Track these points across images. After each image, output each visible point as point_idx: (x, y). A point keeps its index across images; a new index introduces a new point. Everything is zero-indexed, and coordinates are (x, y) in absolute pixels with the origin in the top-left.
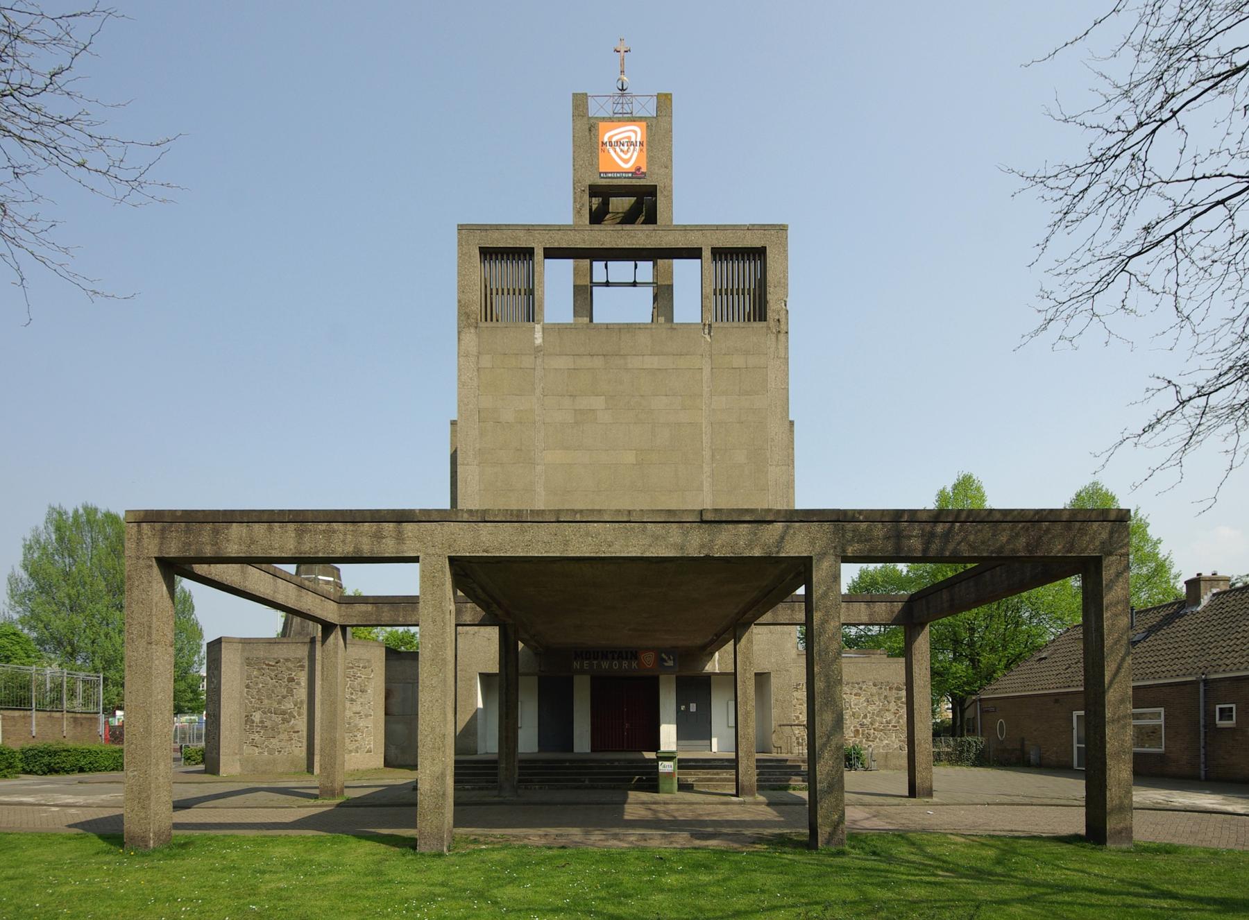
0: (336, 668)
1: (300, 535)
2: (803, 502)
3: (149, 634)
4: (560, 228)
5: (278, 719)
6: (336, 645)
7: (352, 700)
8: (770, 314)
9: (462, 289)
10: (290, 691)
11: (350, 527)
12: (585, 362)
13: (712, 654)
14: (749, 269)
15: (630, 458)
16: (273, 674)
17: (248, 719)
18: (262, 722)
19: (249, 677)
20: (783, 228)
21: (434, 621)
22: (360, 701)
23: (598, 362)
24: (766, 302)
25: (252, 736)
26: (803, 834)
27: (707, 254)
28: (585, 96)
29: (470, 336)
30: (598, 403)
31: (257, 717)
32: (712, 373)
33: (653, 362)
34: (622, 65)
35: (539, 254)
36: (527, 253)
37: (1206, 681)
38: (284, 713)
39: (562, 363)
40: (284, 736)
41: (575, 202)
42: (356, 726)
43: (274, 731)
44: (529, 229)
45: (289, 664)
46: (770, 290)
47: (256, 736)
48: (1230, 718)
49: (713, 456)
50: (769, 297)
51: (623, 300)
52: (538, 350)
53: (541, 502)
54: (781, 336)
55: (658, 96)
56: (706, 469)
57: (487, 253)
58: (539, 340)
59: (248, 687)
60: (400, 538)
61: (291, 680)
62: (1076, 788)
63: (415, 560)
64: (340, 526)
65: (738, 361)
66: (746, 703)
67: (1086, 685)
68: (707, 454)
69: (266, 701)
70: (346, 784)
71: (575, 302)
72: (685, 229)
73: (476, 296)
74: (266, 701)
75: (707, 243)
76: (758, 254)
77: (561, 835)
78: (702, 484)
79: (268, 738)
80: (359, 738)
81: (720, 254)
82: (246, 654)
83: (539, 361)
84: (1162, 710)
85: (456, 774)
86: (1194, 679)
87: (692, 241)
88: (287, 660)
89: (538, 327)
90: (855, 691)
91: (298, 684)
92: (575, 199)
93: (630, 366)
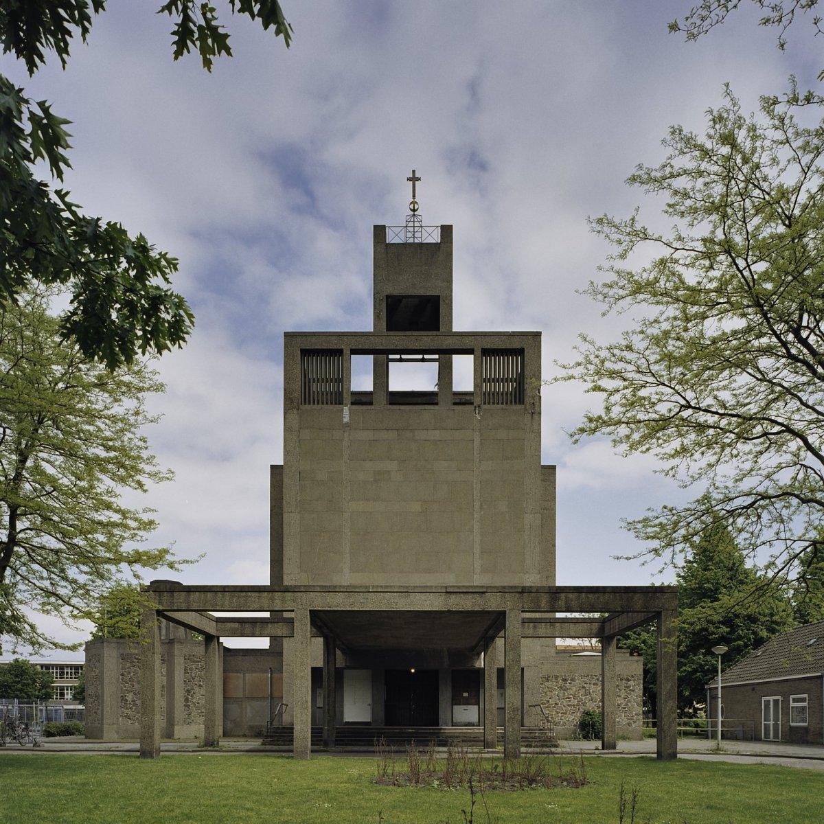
1: (535, 627)
3: (153, 648)
6: (214, 648)
7: (200, 686)
8: (526, 399)
11: (257, 594)
13: (479, 655)
14: (510, 367)
15: (416, 507)
18: (133, 701)
20: (537, 335)
21: (302, 643)
23: (392, 435)
24: (524, 390)
26: (498, 752)
27: (478, 353)
28: (384, 227)
29: (294, 415)
30: (393, 466)
31: (130, 697)
32: (481, 444)
33: (436, 435)
35: (347, 352)
36: (339, 352)
39: (366, 435)
41: (375, 309)
46: (527, 381)
47: (130, 712)
48: (793, 699)
50: (526, 386)
51: (411, 376)
52: (347, 425)
54: (535, 416)
55: (443, 227)
56: (476, 515)
57: (306, 353)
59: (122, 675)
60: (284, 600)
63: (293, 611)
64: (253, 594)
65: (502, 434)
66: (491, 689)
73: (297, 385)
75: (478, 345)
76: (520, 352)
78: (472, 526)
81: (487, 352)
83: (346, 434)
84: (806, 696)
86: (820, 674)
87: (468, 343)
90: (593, 682)
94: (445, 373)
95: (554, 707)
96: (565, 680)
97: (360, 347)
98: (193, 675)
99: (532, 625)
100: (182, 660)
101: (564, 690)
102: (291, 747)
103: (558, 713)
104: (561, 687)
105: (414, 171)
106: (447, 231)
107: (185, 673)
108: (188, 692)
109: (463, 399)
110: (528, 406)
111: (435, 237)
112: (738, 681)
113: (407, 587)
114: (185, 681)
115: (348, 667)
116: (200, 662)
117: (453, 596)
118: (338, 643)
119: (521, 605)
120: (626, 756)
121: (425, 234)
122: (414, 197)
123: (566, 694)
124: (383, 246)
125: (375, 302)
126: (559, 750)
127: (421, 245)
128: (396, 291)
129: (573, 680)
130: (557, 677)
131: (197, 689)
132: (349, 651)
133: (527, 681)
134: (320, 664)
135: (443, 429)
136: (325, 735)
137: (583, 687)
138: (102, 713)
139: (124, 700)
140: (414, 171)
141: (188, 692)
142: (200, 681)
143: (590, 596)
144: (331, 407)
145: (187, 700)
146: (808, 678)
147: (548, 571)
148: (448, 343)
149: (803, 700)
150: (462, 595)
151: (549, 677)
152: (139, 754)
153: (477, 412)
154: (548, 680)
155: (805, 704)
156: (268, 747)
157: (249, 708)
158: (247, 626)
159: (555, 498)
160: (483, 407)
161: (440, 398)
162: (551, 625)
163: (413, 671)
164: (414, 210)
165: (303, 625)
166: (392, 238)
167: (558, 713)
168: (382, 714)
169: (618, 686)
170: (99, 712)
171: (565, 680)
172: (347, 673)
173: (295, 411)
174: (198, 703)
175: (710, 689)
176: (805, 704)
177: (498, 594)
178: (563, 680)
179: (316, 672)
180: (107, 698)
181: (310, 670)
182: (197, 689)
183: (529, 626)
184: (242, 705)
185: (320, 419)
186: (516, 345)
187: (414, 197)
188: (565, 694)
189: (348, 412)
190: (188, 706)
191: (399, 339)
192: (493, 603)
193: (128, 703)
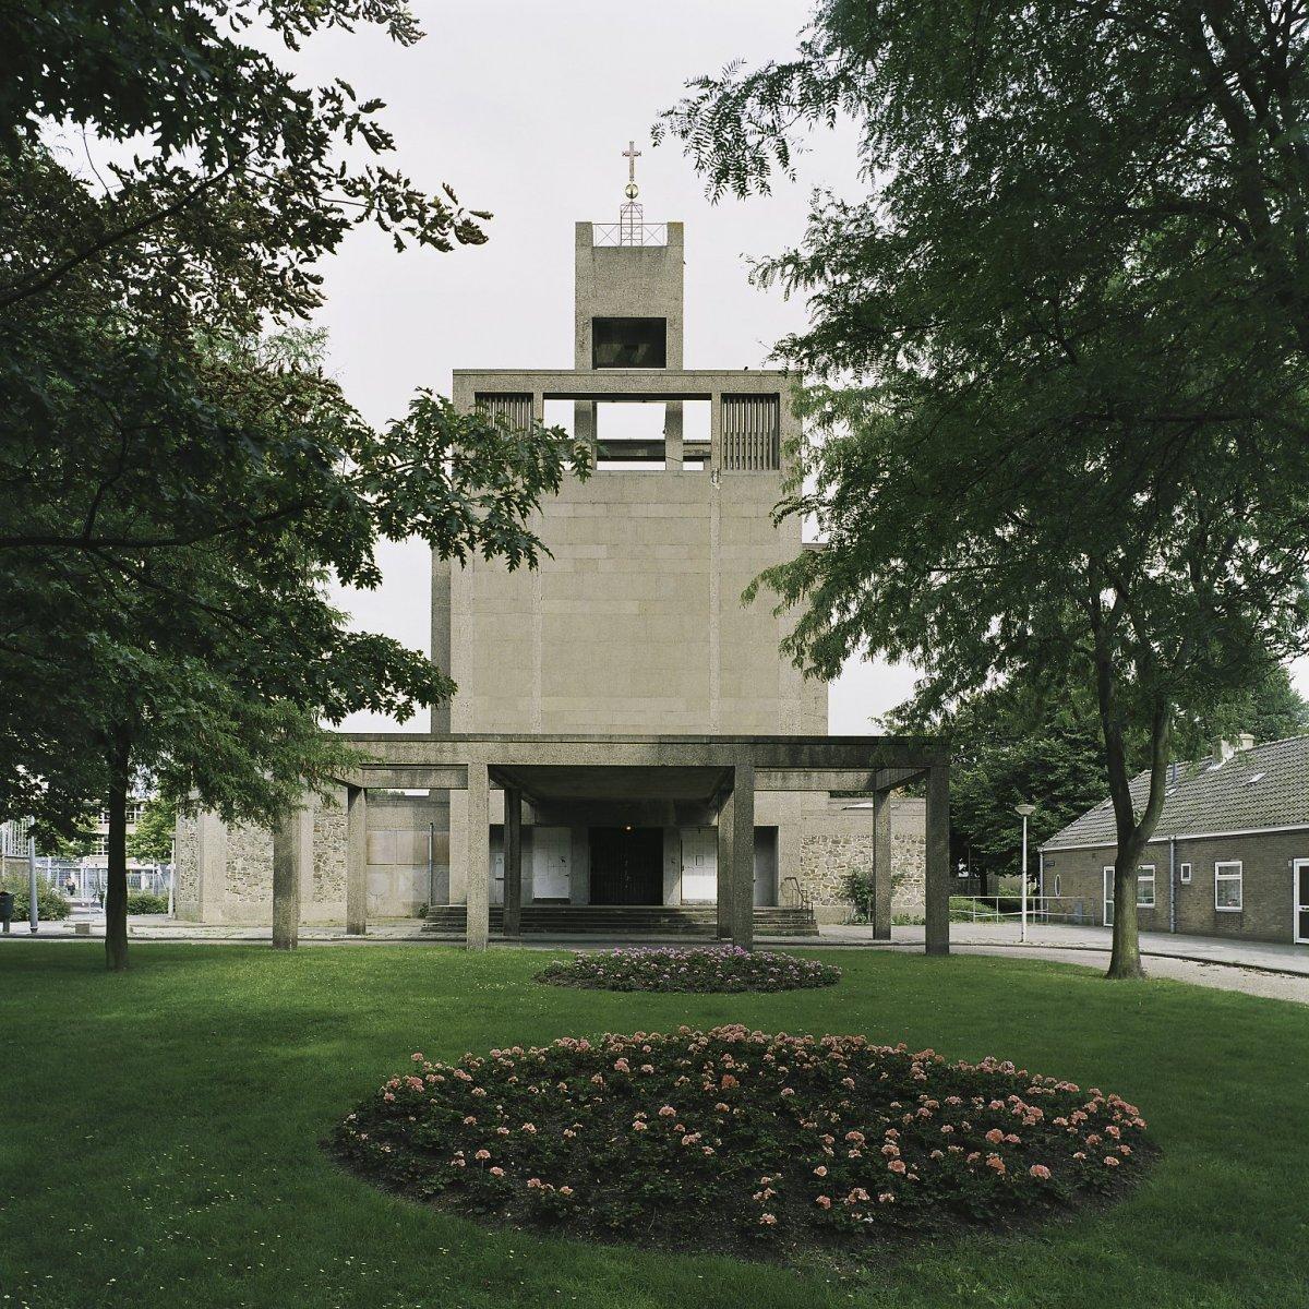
0: (619, 960)
4: (560, 373)
12: (587, 510)
15: (632, 607)
17: (230, 866)
23: (600, 510)
25: (234, 883)
27: (717, 398)
30: (602, 552)
31: (239, 864)
34: (632, 170)
35: (538, 396)
36: (529, 397)
37: (1175, 841)
44: (528, 374)
47: (239, 883)
49: (720, 606)
53: (537, 730)
55: (670, 225)
62: (1105, 939)
67: (1119, 840)
68: (714, 605)
69: (247, 849)
72: (694, 374)
75: (717, 389)
81: (727, 398)
85: (490, 920)
92: (577, 332)
93: (633, 514)
94: (674, 420)
97: (557, 390)
98: (326, 834)
102: (461, 936)
103: (826, 887)
105: (632, 143)
106: (676, 229)
109: (697, 452)
110: (785, 472)
111: (659, 238)
112: (652, 910)
113: (611, 736)
115: (541, 825)
117: (669, 747)
118: (524, 794)
120: (846, 948)
121: (646, 235)
122: (632, 177)
124: (589, 250)
125: (577, 326)
126: (814, 938)
127: (641, 249)
128: (607, 311)
132: (540, 804)
134: (500, 819)
135: (668, 502)
136: (507, 919)
138: (201, 887)
139: (230, 866)
140: (632, 143)
143: (842, 748)
145: (317, 868)
146: (1208, 839)
148: (676, 386)
149: (1223, 871)
152: (270, 943)
155: (1152, 878)
156: (433, 935)
157: (401, 876)
158: (405, 774)
160: (723, 472)
161: (669, 451)
164: (631, 196)
165: (479, 776)
166: (601, 238)
167: (826, 887)
168: (584, 880)
169: (908, 850)
170: (197, 884)
172: (538, 832)
175: (1044, 853)
176: (1152, 878)
178: (834, 842)
179: (496, 832)
180: (207, 865)
181: (487, 830)
186: (769, 389)
187: (632, 177)
190: (320, 877)
191: (610, 379)
192: (722, 758)
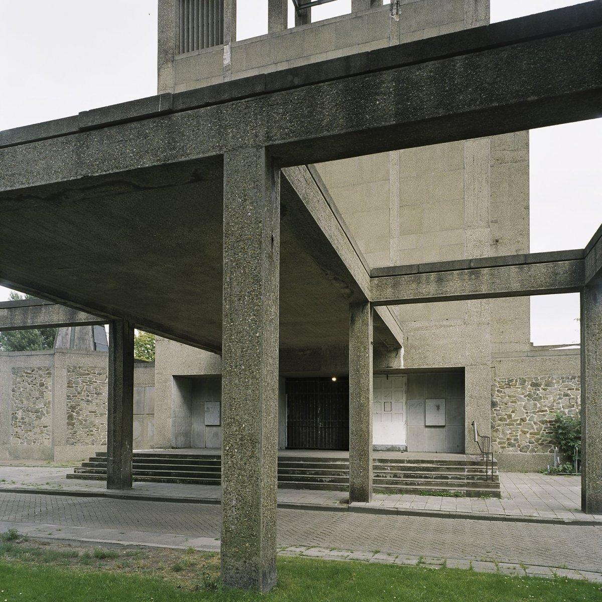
1: (440, 281)
2: (537, 246)
5: (34, 416)
7: (88, 401)
9: (162, 29)
10: (42, 393)
16: (30, 380)
18: (23, 419)
19: (14, 383)
22: (95, 402)
25: (16, 430)
26: (215, 547)
29: (169, 69)
31: (20, 414)
38: (37, 411)
40: (37, 430)
42: (92, 423)
43: (29, 427)
45: (41, 372)
58: (227, 60)
59: (13, 391)
61: (42, 385)
69: (25, 402)
70: (424, 424)
71: (269, 18)
74: (25, 402)
77: (525, 452)
79: (27, 431)
80: (95, 432)
82: (12, 365)
88: (40, 369)
89: (227, 48)
91: (47, 388)
95: (520, 424)
96: (536, 385)
98: (79, 390)
99: (433, 276)
100: (65, 372)
101: (535, 399)
103: (524, 433)
104: (529, 396)
107: (68, 387)
108: (73, 408)
114: (68, 396)
116: (89, 374)
119: (262, 132)
123: (538, 405)
129: (548, 384)
130: (523, 382)
131: (83, 404)
133: (470, 385)
137: (567, 395)
141: (73, 408)
142: (88, 396)
144: (210, 49)
145: (70, 417)
147: (518, 242)
150: (114, 130)
151: (512, 381)
153: (394, 11)
154: (509, 386)
159: (528, 146)
162: (471, 274)
163: (334, 379)
167: (524, 433)
171: (536, 385)
173: (170, 65)
174: (86, 421)
177: (202, 110)
178: (533, 385)
182: (83, 404)
183: (428, 279)
184: (143, 422)
185: (198, 68)
188: (535, 405)
189: (229, 51)
190: (73, 425)
193: (18, 420)
